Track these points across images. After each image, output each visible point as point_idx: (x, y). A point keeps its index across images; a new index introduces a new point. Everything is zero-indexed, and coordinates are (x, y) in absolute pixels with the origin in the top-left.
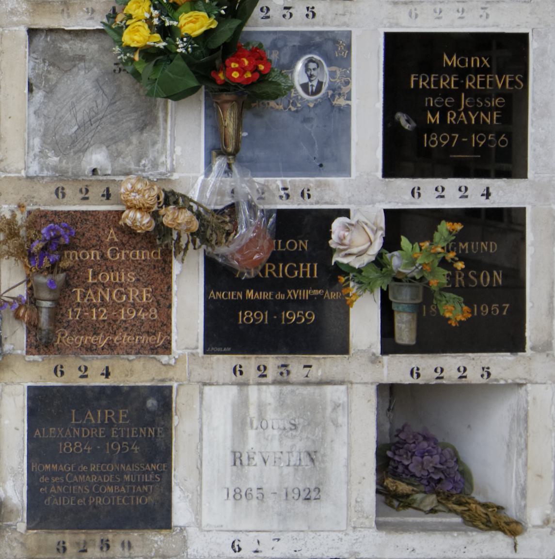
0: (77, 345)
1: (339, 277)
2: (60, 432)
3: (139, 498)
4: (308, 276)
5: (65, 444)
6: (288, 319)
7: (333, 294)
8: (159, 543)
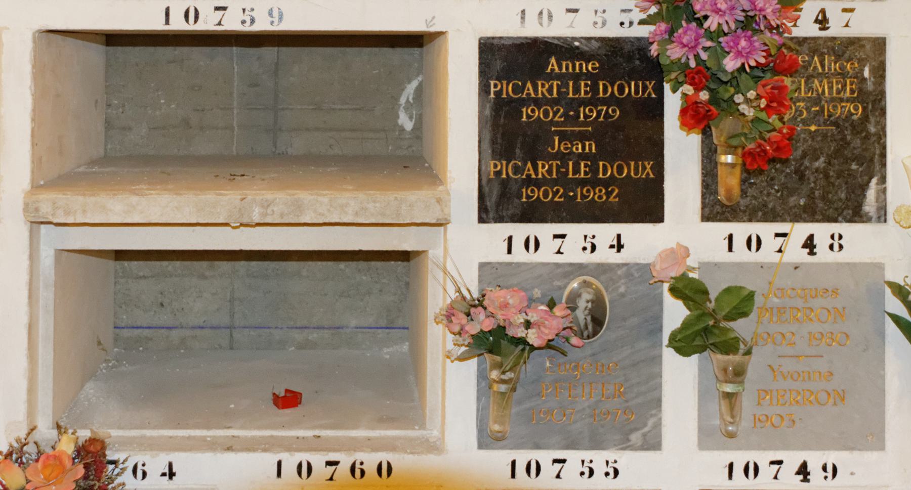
0: (613, 117)
1: (538, 162)
2: (650, 87)
3: (508, 84)
4: (570, 70)
5: (597, 191)
6: (585, 196)
7: (543, 167)
8: (773, 191)
